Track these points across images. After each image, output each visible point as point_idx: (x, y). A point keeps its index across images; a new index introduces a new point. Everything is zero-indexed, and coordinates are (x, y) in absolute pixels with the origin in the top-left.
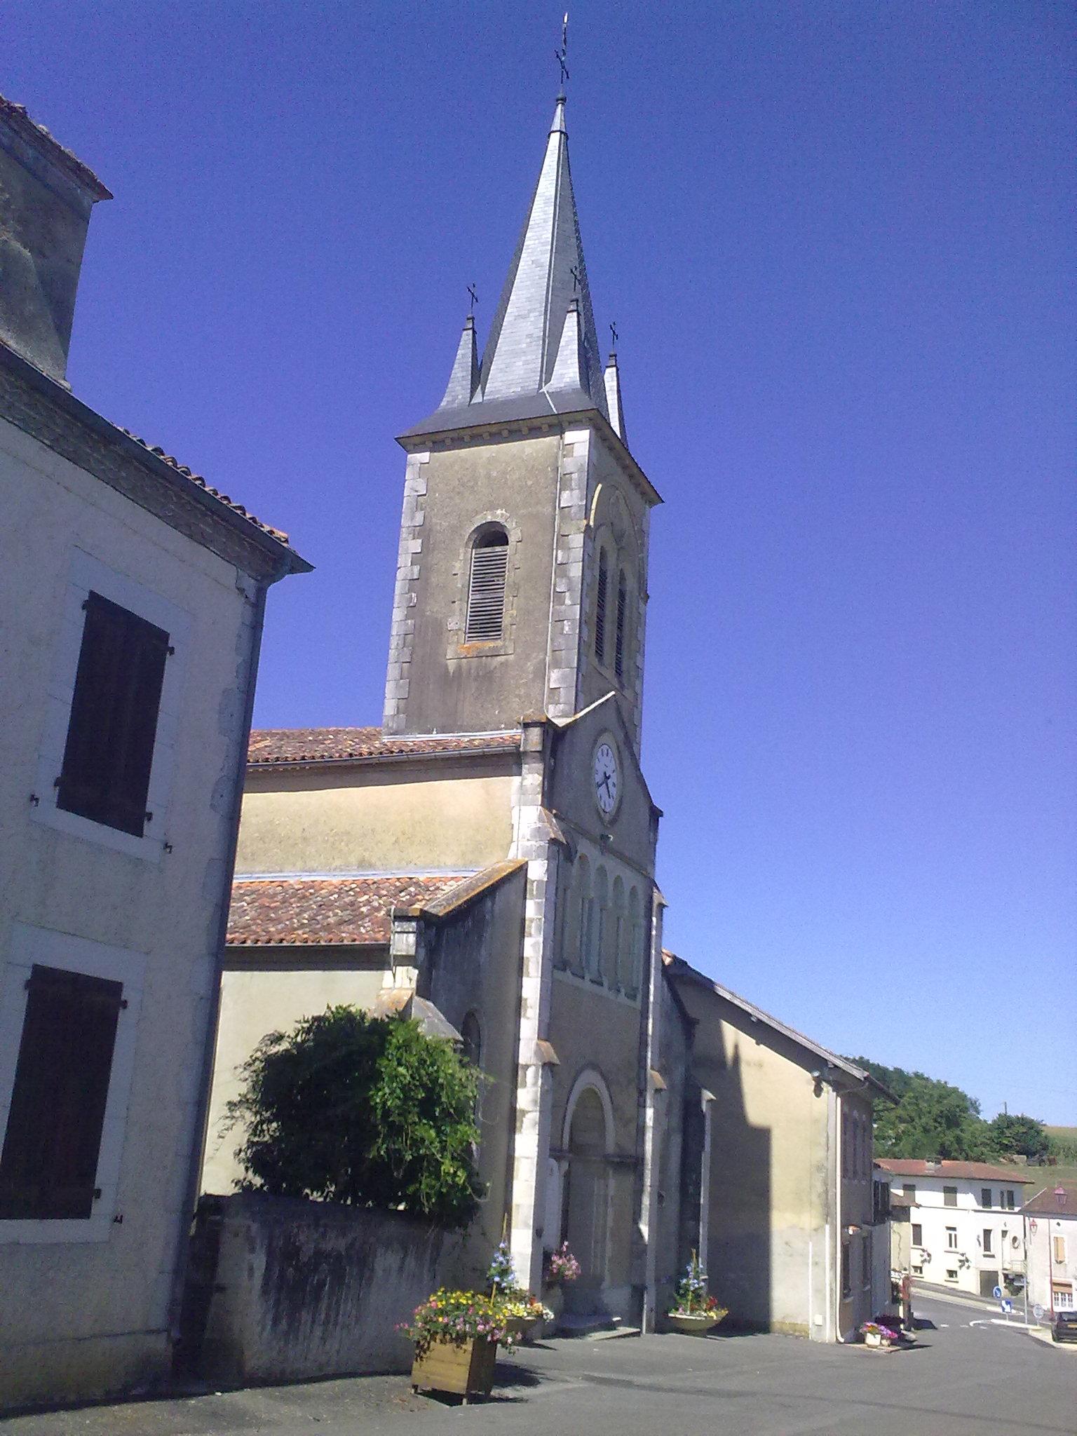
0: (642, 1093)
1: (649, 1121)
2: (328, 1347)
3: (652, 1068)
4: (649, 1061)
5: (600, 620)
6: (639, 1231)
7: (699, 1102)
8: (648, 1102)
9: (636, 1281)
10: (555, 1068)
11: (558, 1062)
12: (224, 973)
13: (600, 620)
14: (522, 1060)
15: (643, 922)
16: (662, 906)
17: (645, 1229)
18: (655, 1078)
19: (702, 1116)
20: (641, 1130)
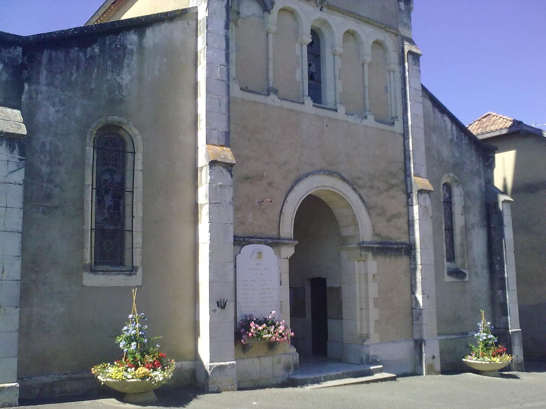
0: (409, 195)
1: (416, 216)
2: (137, 371)
3: (416, 175)
4: (412, 170)
5: (118, 271)
6: (416, 299)
7: (497, 203)
8: (415, 201)
9: (417, 337)
10: (431, 194)
11: (432, 189)
12: (26, 134)
13: (118, 271)
14: (200, 165)
15: (398, 69)
16: (416, 57)
17: (419, 296)
18: (420, 182)
19: (500, 214)
20: (410, 224)
